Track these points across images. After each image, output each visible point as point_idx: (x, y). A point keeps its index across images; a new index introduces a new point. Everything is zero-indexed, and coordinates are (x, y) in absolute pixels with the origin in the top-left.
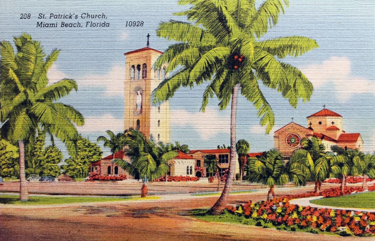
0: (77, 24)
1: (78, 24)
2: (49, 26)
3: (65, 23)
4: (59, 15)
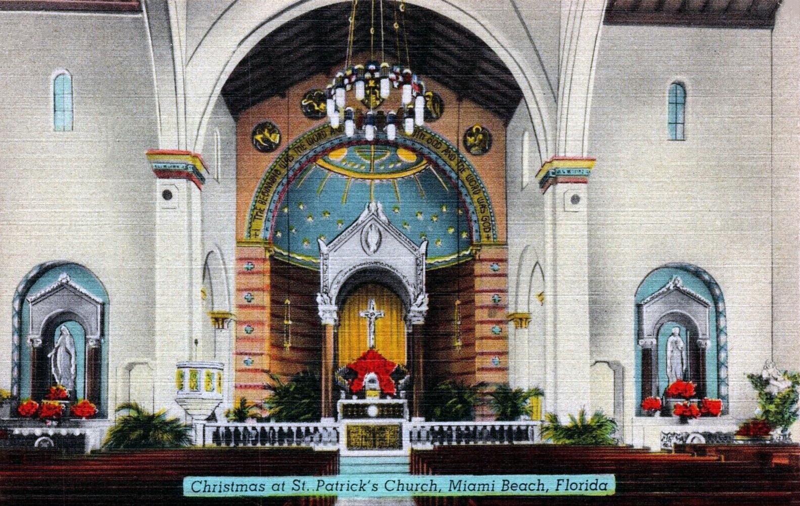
0: (429, 486)
1: (539, 485)
2: (476, 489)
3: (511, 483)
4: (337, 484)
